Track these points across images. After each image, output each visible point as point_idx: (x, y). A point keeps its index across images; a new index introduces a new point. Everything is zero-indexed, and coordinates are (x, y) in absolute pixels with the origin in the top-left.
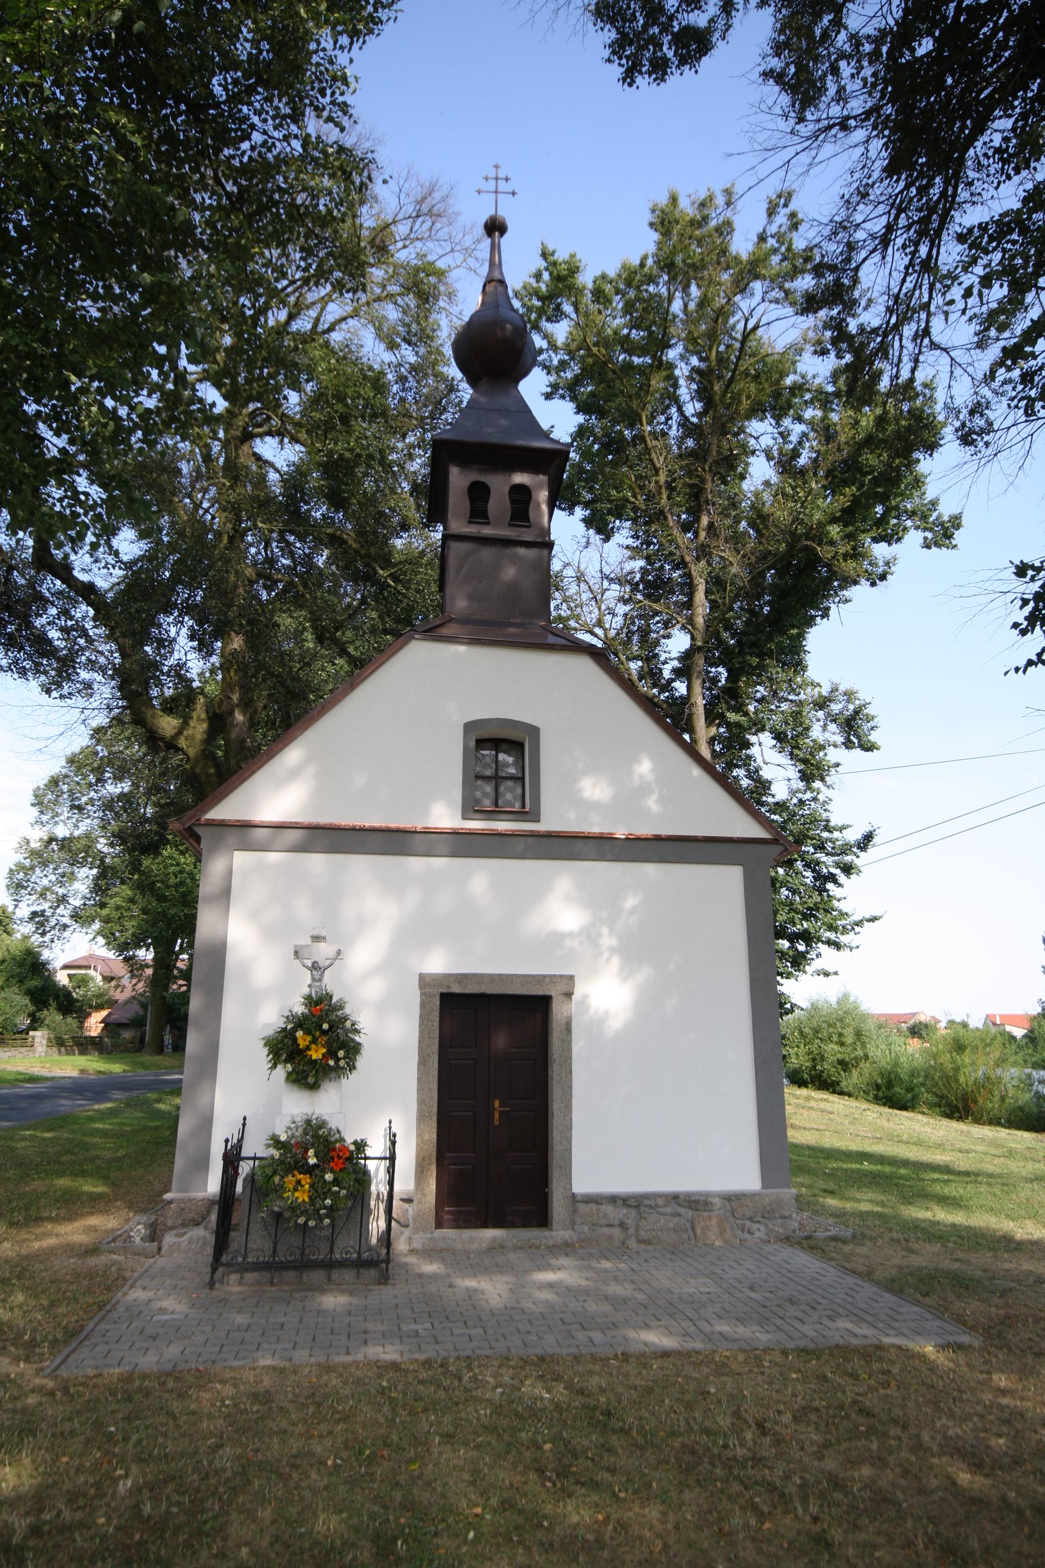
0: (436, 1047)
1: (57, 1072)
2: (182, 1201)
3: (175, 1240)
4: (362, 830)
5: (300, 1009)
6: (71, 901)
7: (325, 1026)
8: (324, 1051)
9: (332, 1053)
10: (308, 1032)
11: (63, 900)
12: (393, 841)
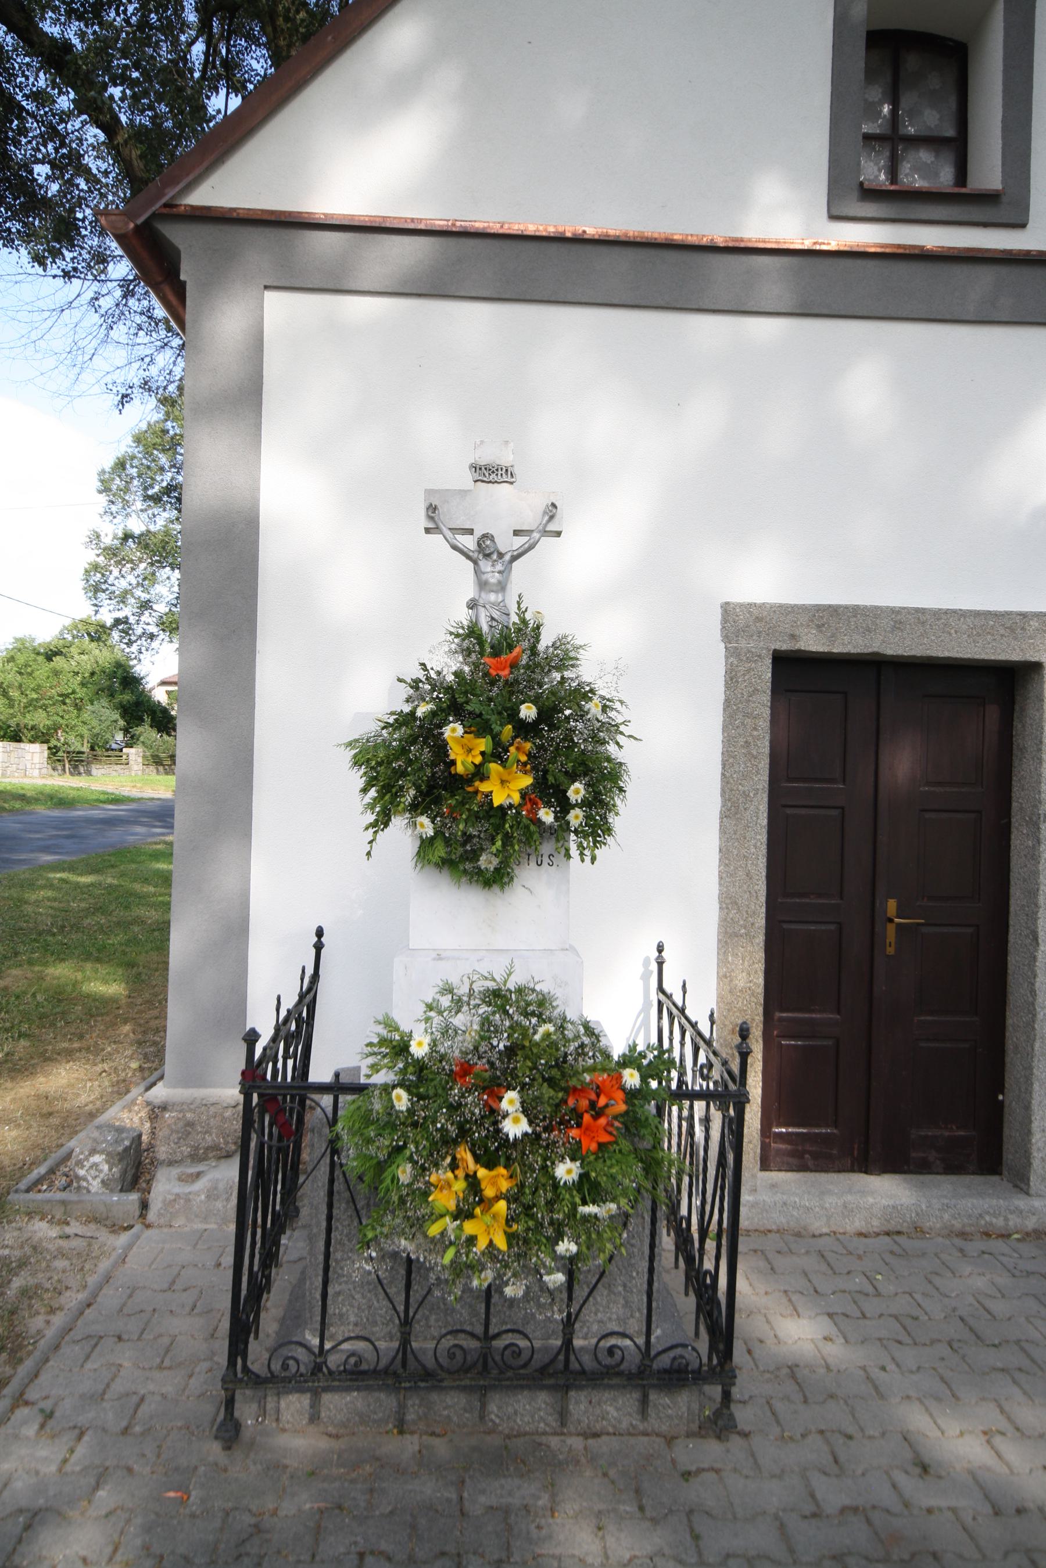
0: (762, 779)
1: (149, 793)
2: (182, 1106)
3: (179, 1189)
4: (579, 240)
5: (447, 664)
6: (155, 607)
7: (528, 712)
8: (527, 781)
9: (548, 790)
10: (478, 726)
11: (145, 605)
12: (664, 271)
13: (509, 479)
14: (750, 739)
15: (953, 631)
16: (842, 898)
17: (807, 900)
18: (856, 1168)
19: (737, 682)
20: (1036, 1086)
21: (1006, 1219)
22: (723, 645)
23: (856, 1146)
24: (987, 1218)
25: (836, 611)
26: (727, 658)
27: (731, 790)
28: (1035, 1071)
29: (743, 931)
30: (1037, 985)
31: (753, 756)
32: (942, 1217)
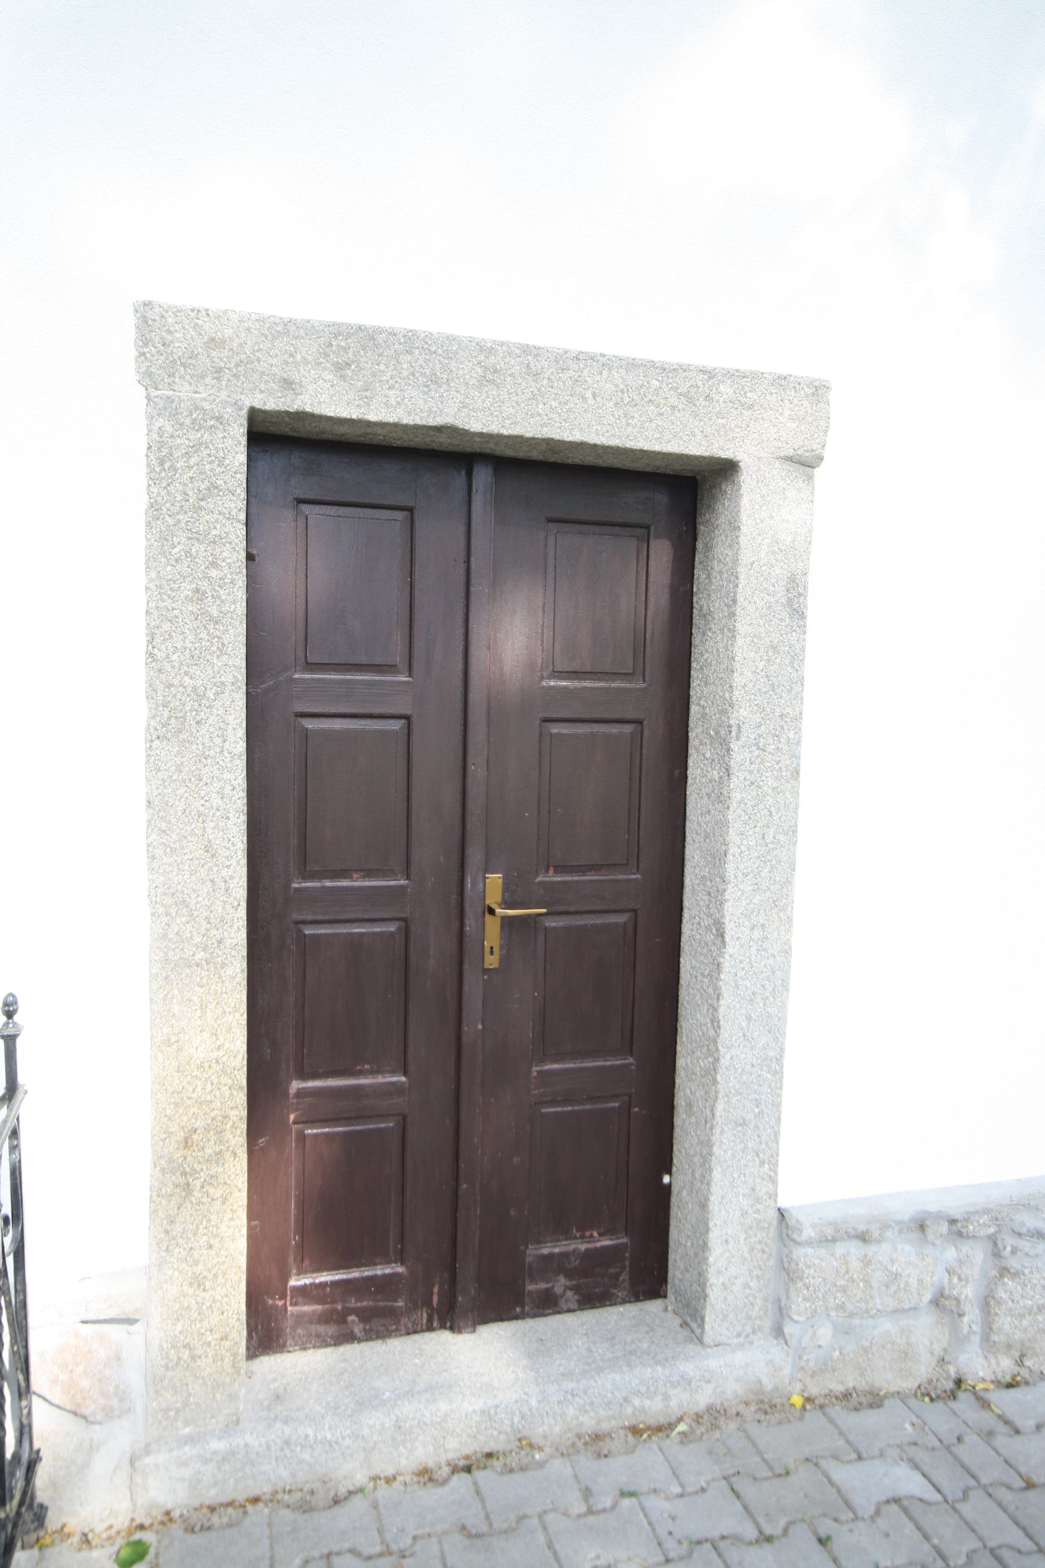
14: (204, 585)
15: (589, 394)
16: (408, 878)
17: (345, 883)
18: (435, 1325)
19: (173, 468)
20: (717, 1174)
21: (666, 1398)
22: (143, 392)
23: (436, 1290)
24: (637, 1402)
26: (151, 418)
27: (170, 686)
28: (715, 1149)
29: (201, 955)
30: (721, 1010)
31: (211, 618)
32: (563, 1415)
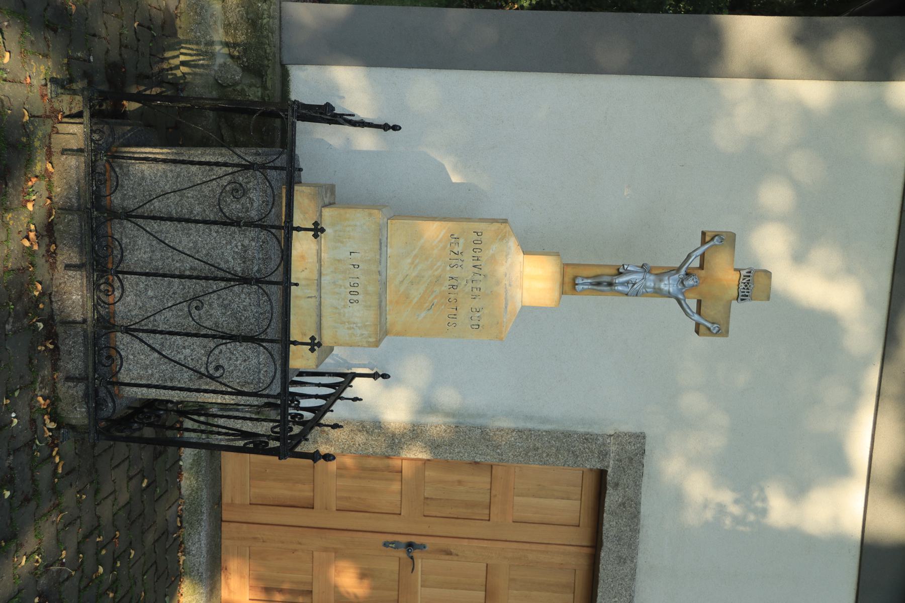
13: (740, 297)
14: (540, 451)
25: (635, 517)
